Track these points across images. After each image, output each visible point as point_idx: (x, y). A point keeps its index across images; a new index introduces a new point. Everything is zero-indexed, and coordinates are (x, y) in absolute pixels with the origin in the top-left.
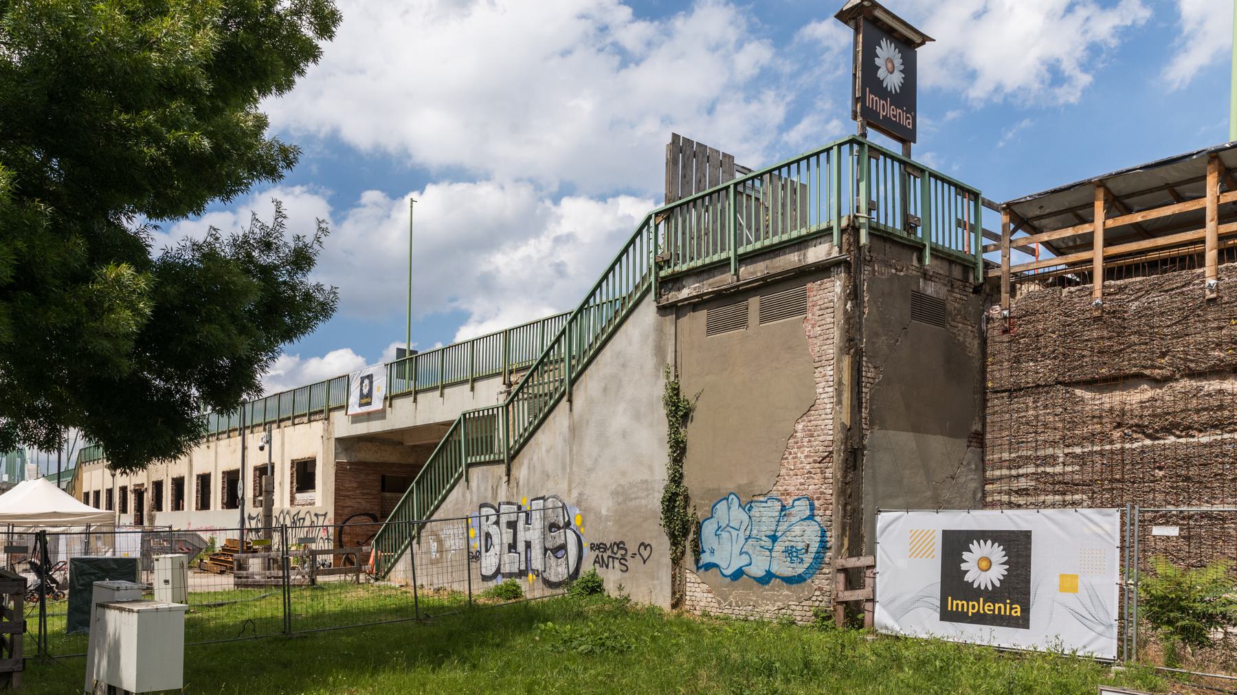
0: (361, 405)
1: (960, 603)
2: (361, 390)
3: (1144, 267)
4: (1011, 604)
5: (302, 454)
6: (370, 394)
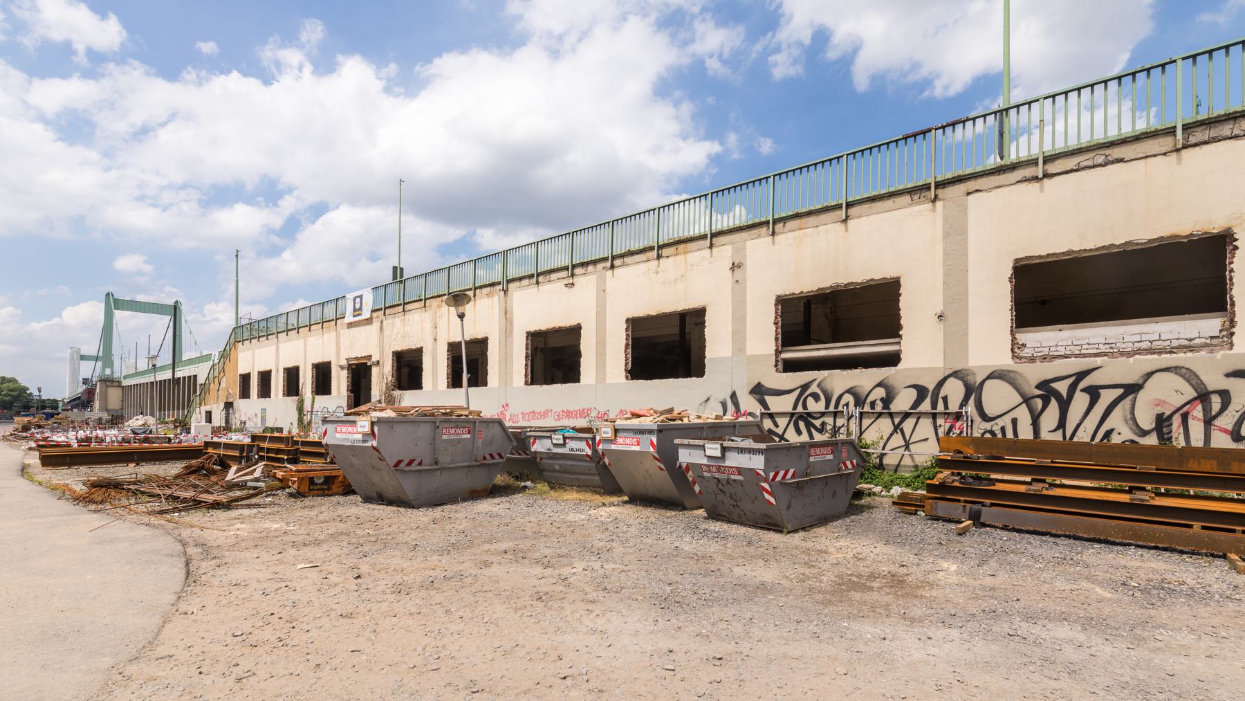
0: (354, 316)
2: (354, 306)
5: (359, 352)
6: (361, 309)
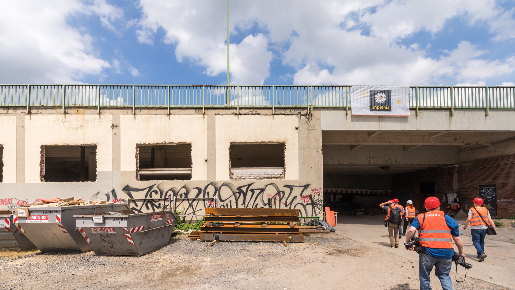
1: (375, 107)
3: (53, 212)
4: (387, 106)
